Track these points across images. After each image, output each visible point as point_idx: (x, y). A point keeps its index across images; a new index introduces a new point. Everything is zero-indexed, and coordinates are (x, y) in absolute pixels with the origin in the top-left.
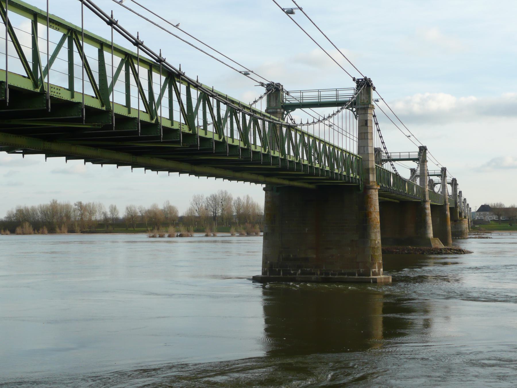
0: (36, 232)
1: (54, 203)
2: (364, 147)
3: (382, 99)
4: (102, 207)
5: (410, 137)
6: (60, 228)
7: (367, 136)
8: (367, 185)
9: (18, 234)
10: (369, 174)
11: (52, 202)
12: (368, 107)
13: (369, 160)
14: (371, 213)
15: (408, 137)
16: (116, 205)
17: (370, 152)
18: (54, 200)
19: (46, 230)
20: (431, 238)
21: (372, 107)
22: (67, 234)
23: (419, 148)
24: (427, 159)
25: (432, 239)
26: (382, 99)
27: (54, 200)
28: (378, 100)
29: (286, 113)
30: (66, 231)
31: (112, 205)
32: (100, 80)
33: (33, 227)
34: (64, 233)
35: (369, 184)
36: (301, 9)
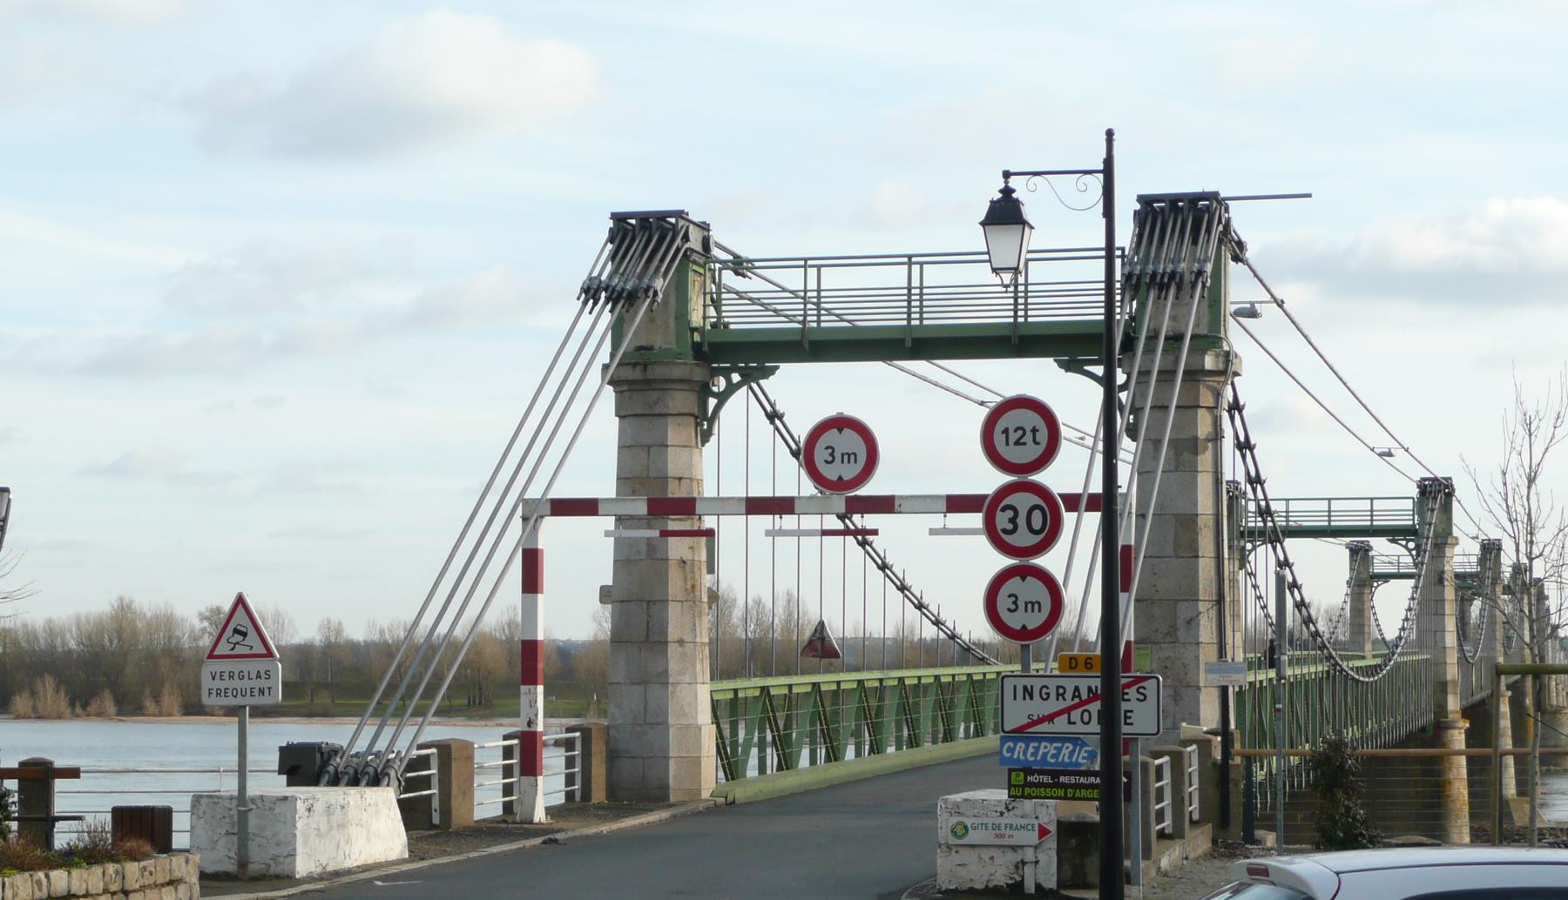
0: (78, 710)
1: (122, 609)
2: (1435, 632)
3: (1276, 301)
4: (284, 622)
5: (1390, 454)
6: (157, 699)
7: (1443, 607)
8: (1442, 720)
9: (18, 717)
10: (1446, 694)
11: (116, 605)
12: (1446, 543)
13: (1446, 663)
14: (1450, 783)
15: (1380, 455)
16: (342, 621)
17: (1448, 645)
18: (121, 599)
19: (111, 707)
20: (1510, 797)
21: (1454, 542)
22: (180, 718)
23: (1419, 487)
24: (1456, 532)
25: (1513, 800)
26: (1276, 301)
27: (121, 599)
28: (1392, 450)
29: (1249, 546)
30: (176, 709)
31: (329, 622)
32: (712, 414)
33: (67, 693)
34: (170, 715)
35: (1447, 717)
36: (1280, 304)
